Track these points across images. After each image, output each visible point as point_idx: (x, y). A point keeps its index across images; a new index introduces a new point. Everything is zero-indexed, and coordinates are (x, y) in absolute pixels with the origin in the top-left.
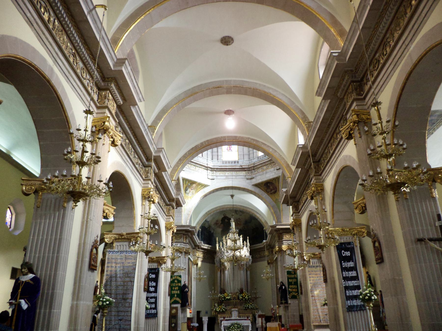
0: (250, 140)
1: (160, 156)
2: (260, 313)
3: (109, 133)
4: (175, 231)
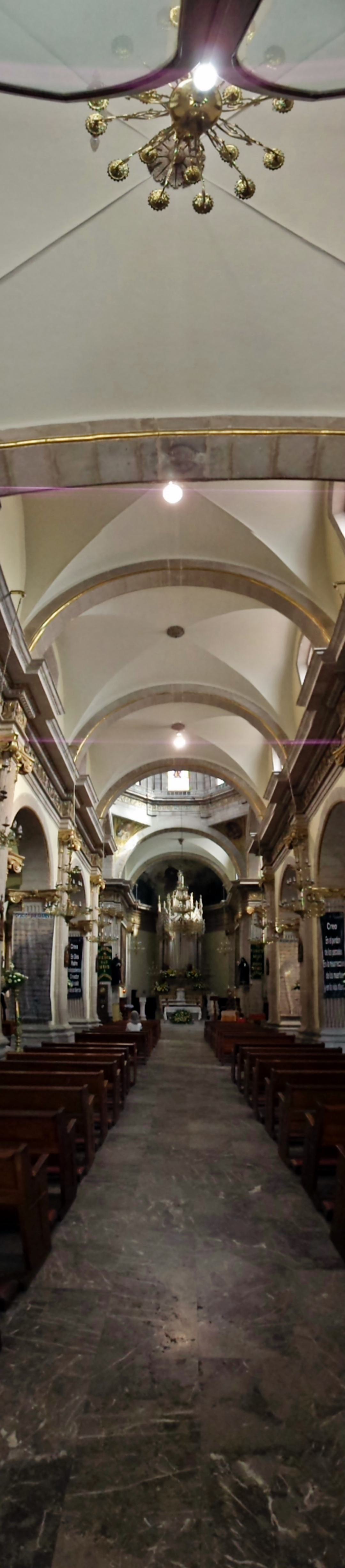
1: (83, 787)
2: (213, 994)
3: (17, 756)
4: (104, 887)
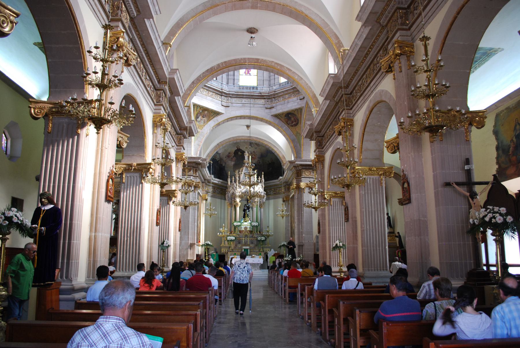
0: (273, 64)
3: (123, 51)
4: (186, 163)
